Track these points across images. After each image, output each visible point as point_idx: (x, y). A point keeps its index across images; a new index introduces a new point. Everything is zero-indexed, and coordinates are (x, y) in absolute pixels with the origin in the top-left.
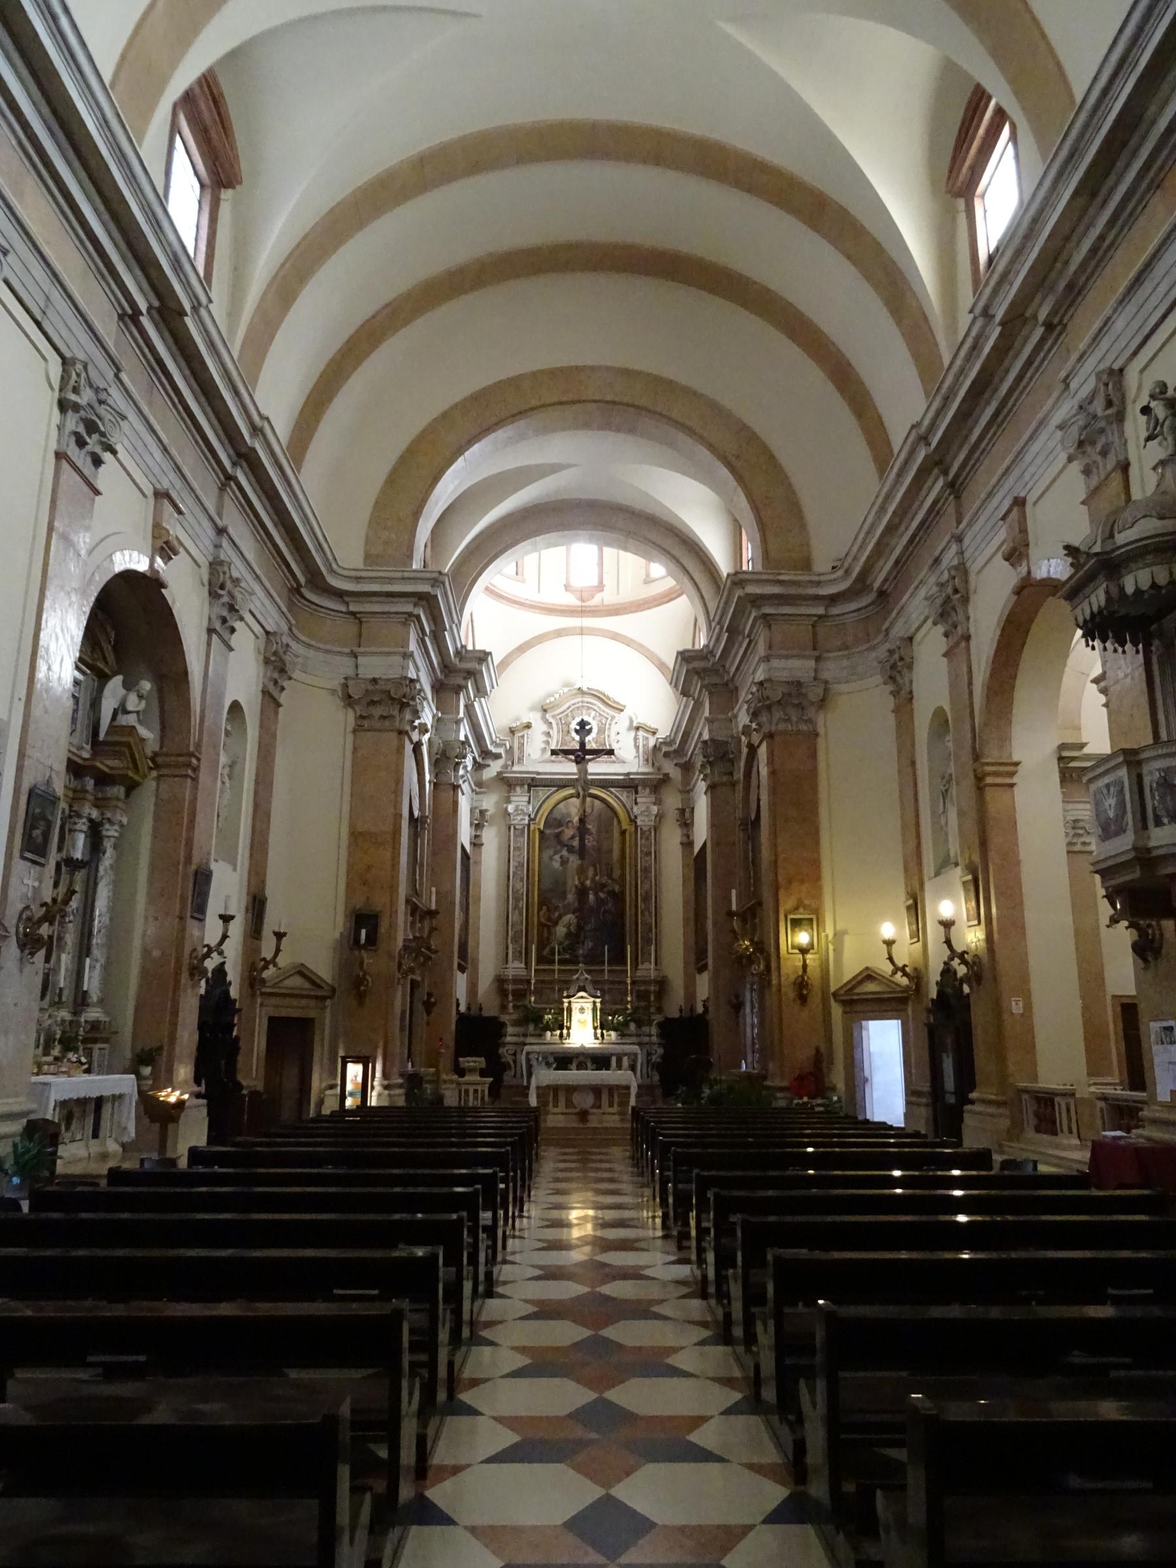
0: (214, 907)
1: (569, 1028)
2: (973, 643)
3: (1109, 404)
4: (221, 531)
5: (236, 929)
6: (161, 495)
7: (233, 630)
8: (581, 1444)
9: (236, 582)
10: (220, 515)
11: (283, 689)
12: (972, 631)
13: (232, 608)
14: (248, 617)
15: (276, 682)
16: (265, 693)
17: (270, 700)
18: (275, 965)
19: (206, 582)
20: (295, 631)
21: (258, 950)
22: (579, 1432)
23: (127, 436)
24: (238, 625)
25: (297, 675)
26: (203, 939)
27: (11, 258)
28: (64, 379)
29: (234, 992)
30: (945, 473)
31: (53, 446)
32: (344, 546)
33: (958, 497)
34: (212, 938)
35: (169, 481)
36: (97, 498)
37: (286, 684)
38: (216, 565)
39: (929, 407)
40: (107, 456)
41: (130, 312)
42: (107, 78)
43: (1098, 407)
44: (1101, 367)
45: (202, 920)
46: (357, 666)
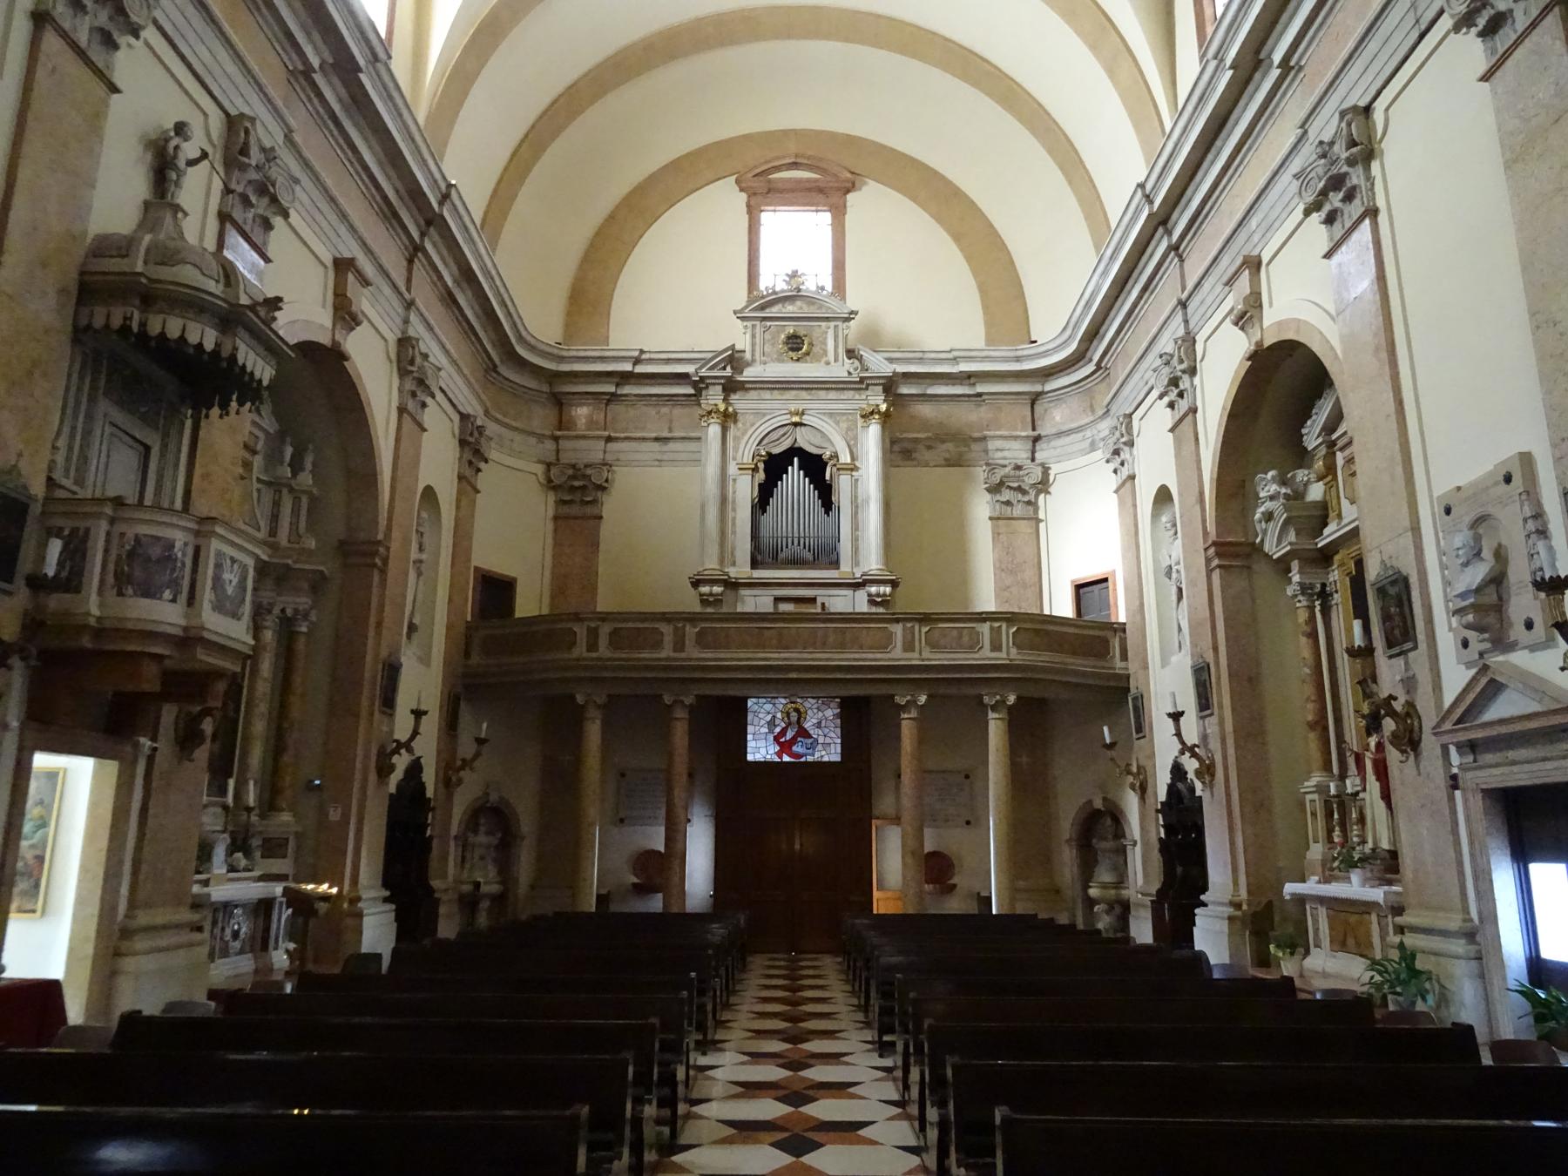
0: (405, 700)
1: (642, 352)
2: (1199, 415)
3: (1352, 143)
4: (409, 305)
5: (431, 726)
6: (343, 266)
7: (424, 405)
8: (813, 1129)
9: (269, 154)
10: (409, 290)
11: (479, 470)
12: (1381, 202)
13: (421, 382)
14: (439, 396)
15: (470, 463)
16: (461, 478)
17: (467, 484)
18: (410, 750)
19: (393, 356)
20: (493, 413)
21: (453, 752)
22: (811, 1093)
23: (302, 200)
24: (429, 400)
25: (493, 455)
26: (392, 732)
27: (442, 373)
28: (462, 430)
29: (430, 793)
30: (1169, 233)
31: (395, 404)
32: (539, 316)
33: (1182, 260)
34: (402, 731)
35: (351, 249)
36: (115, 96)
37: (482, 465)
38: (405, 342)
39: (1202, 73)
40: (278, 221)
41: (301, 67)
42: (478, 223)
43: (1340, 151)
44: (1345, 106)
45: (392, 715)
46: (558, 451)
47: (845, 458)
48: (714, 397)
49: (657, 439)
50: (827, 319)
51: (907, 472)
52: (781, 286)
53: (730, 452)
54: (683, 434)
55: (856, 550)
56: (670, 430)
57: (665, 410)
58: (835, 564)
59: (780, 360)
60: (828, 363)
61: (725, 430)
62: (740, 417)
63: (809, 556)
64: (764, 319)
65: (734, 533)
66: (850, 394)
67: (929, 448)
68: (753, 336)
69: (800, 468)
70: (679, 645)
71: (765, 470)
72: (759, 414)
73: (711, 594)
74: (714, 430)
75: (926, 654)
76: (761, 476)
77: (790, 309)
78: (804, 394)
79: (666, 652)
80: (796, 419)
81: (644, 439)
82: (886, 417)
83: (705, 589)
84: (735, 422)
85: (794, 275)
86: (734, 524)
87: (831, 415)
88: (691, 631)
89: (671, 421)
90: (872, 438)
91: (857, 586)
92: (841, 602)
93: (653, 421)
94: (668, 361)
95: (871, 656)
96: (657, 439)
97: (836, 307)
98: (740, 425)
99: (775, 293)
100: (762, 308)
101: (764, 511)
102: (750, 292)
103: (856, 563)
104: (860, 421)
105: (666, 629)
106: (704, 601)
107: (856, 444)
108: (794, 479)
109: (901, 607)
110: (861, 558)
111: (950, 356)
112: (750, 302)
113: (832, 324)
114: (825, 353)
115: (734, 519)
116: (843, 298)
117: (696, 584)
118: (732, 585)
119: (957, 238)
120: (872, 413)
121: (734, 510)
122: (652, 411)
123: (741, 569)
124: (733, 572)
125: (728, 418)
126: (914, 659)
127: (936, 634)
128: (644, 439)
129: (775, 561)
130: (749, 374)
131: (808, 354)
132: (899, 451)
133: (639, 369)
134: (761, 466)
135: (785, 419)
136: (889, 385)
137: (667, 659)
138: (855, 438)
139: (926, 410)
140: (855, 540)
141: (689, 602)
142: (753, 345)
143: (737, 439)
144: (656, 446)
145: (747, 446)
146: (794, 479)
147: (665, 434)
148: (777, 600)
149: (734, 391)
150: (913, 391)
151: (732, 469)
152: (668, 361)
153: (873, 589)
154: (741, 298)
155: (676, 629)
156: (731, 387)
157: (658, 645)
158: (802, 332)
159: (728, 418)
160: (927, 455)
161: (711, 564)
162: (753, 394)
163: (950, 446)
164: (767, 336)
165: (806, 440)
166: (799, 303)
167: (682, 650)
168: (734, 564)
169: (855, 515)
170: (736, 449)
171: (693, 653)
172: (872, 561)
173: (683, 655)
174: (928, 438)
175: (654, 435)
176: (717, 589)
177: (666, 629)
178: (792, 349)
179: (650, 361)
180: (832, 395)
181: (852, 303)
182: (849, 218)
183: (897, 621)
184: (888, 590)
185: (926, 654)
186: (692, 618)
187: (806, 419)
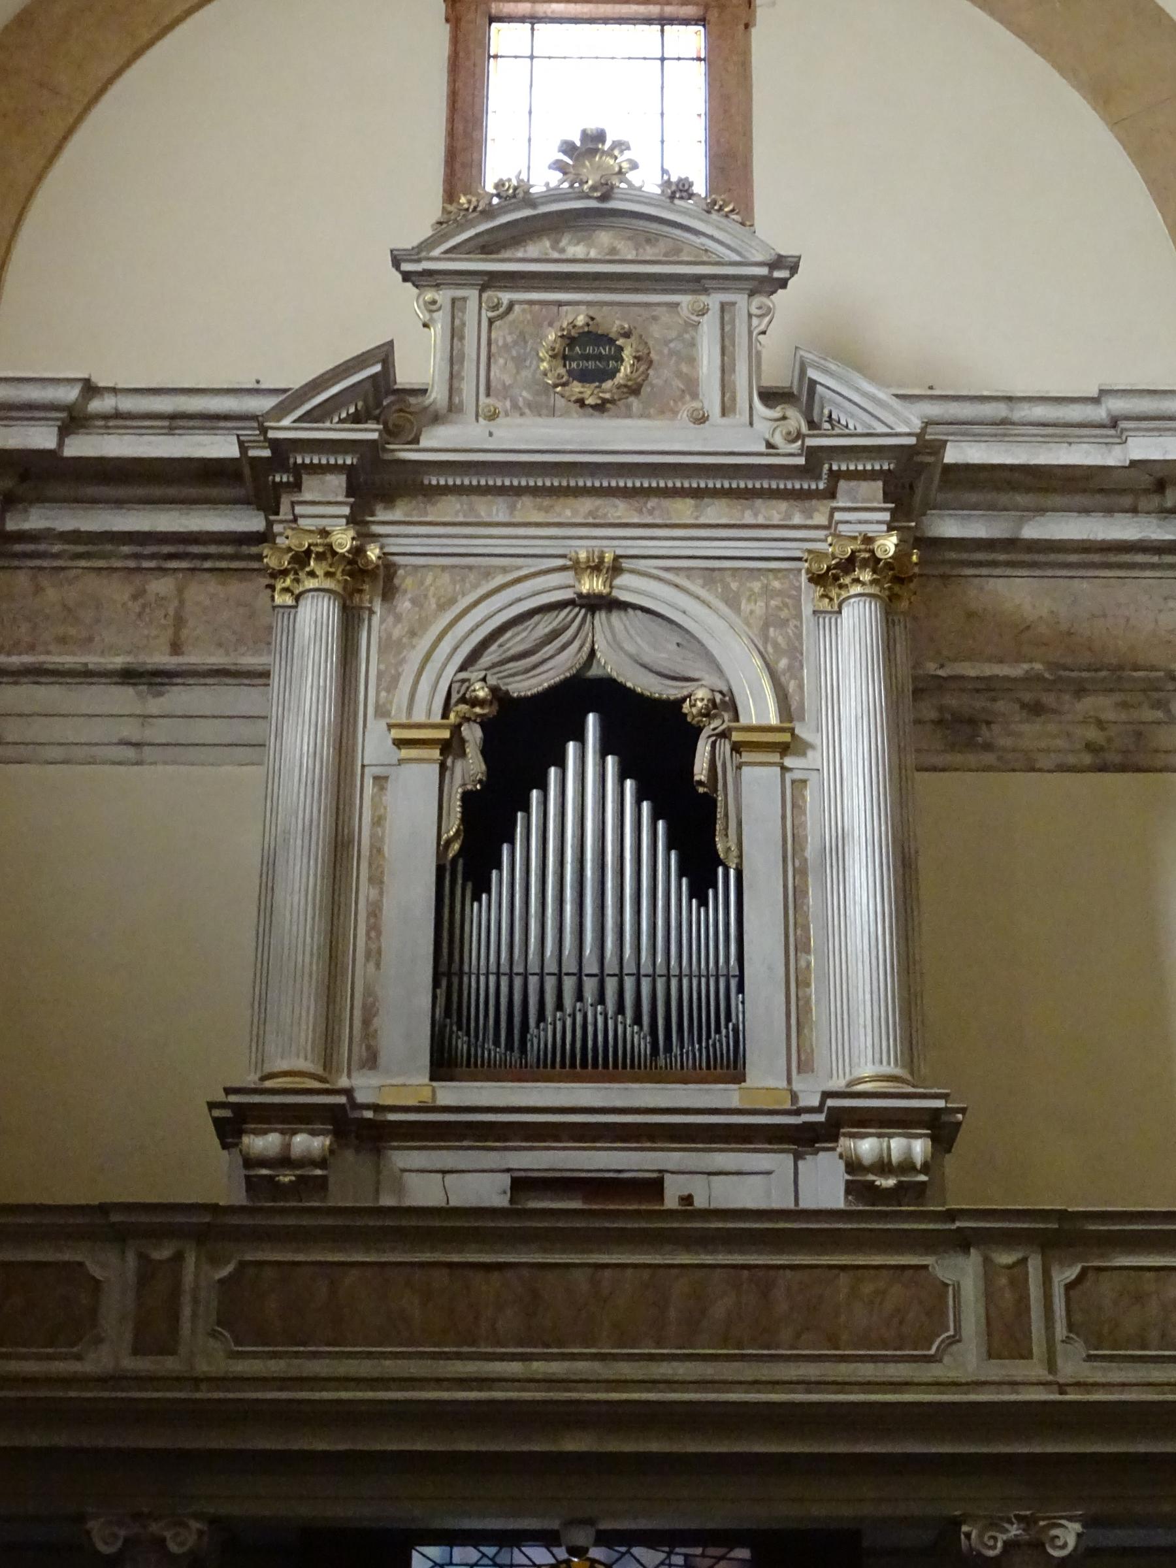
1: (90, 389)
47: (759, 709)
48: (321, 511)
49: (128, 676)
50: (698, 285)
51: (963, 791)
52: (544, 179)
53: (369, 692)
54: (217, 659)
55: (798, 1016)
56: (176, 648)
57: (161, 586)
58: (731, 1067)
59: (536, 409)
60: (701, 419)
61: (351, 620)
62: (406, 582)
63: (640, 1041)
64: (491, 281)
65: (375, 955)
66: (775, 512)
67: (1036, 710)
68: (455, 333)
69: (604, 750)
70: (155, 1332)
71: (487, 751)
72: (465, 567)
73: (285, 1161)
74: (315, 617)
75: (1072, 1367)
76: (472, 767)
77: (577, 252)
78: (619, 510)
79: (109, 1354)
80: (592, 585)
81: (87, 675)
82: (894, 581)
83: (264, 1143)
84: (389, 593)
85: (591, 145)
86: (375, 928)
87: (710, 576)
88: (201, 1275)
89: (179, 621)
90: (849, 652)
91: (805, 1138)
92: (754, 1183)
93: (121, 621)
94: (176, 422)
95: (867, 1371)
96: (128, 676)
97: (721, 244)
98: (404, 604)
99: (529, 201)
100: (487, 246)
101: (482, 886)
102: (450, 196)
103: (802, 1060)
104: (810, 597)
105: (112, 1269)
106: (260, 1179)
107: (795, 669)
108: (586, 789)
109: (965, 1188)
110: (819, 1037)
111: (1100, 413)
112: (444, 229)
113: (714, 300)
114: (691, 388)
115: (375, 912)
116: (747, 222)
117: (233, 1122)
118: (366, 1132)
119: (1102, 94)
120: (849, 564)
121: (377, 880)
122: (117, 592)
123: (397, 1078)
124: (367, 1087)
125: (363, 582)
126: (1027, 1381)
127: (1106, 1289)
128: (87, 675)
129: (521, 1058)
130: (438, 442)
131: (634, 390)
132: (943, 719)
133: (80, 447)
134: (473, 734)
135: (556, 586)
136: (912, 477)
137: (103, 1380)
138: (795, 652)
139: (1019, 595)
140: (797, 982)
141: (215, 1179)
142: (454, 360)
143: (389, 646)
144: (124, 698)
145: (424, 667)
146: (586, 789)
147: (162, 659)
148: (522, 1184)
149: (388, 498)
150: (977, 528)
151: (374, 744)
152: (176, 422)
153: (867, 1147)
154: (416, 214)
155: (147, 1273)
156: (378, 482)
157: (78, 1327)
158: (614, 324)
159: (363, 582)
160: (1031, 733)
161: (292, 1055)
162: (450, 508)
163: (1101, 704)
164: (501, 334)
165: (625, 655)
166: (604, 238)
167: (167, 1348)
168: (371, 1061)
169: (795, 901)
170: (389, 682)
171: (207, 1354)
172: (859, 1051)
173: (171, 1365)
174: (1031, 680)
175: (118, 661)
176: (308, 1143)
177: (112, 1269)
178: (584, 377)
179: (118, 420)
180: (716, 511)
181: (774, 227)
182: (765, 42)
183: (963, 1242)
184: (920, 1148)
185: (1072, 1367)
186: (207, 1227)
187: (628, 587)
